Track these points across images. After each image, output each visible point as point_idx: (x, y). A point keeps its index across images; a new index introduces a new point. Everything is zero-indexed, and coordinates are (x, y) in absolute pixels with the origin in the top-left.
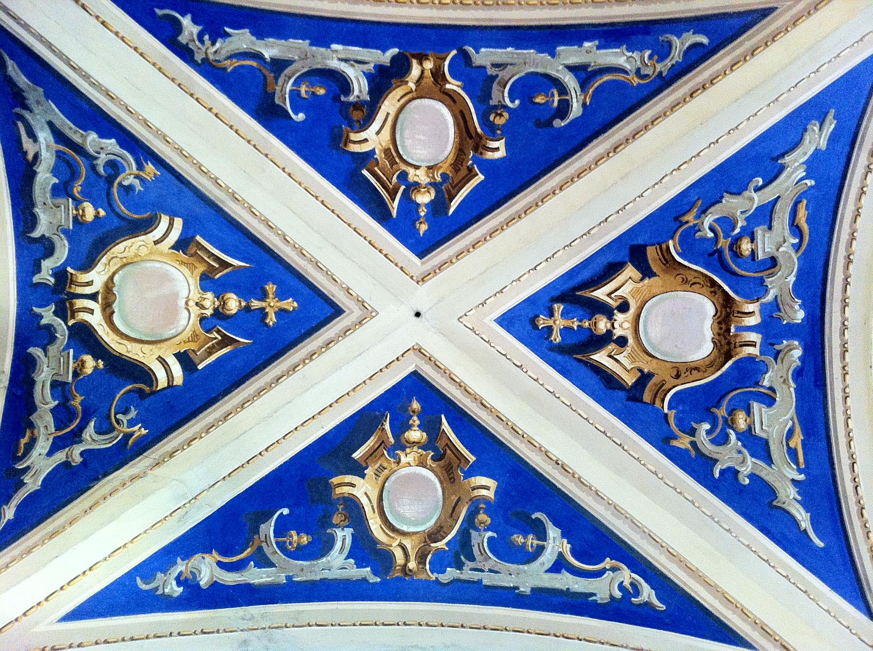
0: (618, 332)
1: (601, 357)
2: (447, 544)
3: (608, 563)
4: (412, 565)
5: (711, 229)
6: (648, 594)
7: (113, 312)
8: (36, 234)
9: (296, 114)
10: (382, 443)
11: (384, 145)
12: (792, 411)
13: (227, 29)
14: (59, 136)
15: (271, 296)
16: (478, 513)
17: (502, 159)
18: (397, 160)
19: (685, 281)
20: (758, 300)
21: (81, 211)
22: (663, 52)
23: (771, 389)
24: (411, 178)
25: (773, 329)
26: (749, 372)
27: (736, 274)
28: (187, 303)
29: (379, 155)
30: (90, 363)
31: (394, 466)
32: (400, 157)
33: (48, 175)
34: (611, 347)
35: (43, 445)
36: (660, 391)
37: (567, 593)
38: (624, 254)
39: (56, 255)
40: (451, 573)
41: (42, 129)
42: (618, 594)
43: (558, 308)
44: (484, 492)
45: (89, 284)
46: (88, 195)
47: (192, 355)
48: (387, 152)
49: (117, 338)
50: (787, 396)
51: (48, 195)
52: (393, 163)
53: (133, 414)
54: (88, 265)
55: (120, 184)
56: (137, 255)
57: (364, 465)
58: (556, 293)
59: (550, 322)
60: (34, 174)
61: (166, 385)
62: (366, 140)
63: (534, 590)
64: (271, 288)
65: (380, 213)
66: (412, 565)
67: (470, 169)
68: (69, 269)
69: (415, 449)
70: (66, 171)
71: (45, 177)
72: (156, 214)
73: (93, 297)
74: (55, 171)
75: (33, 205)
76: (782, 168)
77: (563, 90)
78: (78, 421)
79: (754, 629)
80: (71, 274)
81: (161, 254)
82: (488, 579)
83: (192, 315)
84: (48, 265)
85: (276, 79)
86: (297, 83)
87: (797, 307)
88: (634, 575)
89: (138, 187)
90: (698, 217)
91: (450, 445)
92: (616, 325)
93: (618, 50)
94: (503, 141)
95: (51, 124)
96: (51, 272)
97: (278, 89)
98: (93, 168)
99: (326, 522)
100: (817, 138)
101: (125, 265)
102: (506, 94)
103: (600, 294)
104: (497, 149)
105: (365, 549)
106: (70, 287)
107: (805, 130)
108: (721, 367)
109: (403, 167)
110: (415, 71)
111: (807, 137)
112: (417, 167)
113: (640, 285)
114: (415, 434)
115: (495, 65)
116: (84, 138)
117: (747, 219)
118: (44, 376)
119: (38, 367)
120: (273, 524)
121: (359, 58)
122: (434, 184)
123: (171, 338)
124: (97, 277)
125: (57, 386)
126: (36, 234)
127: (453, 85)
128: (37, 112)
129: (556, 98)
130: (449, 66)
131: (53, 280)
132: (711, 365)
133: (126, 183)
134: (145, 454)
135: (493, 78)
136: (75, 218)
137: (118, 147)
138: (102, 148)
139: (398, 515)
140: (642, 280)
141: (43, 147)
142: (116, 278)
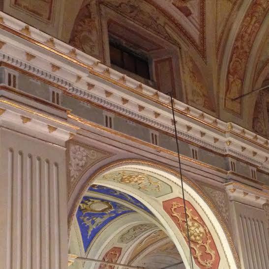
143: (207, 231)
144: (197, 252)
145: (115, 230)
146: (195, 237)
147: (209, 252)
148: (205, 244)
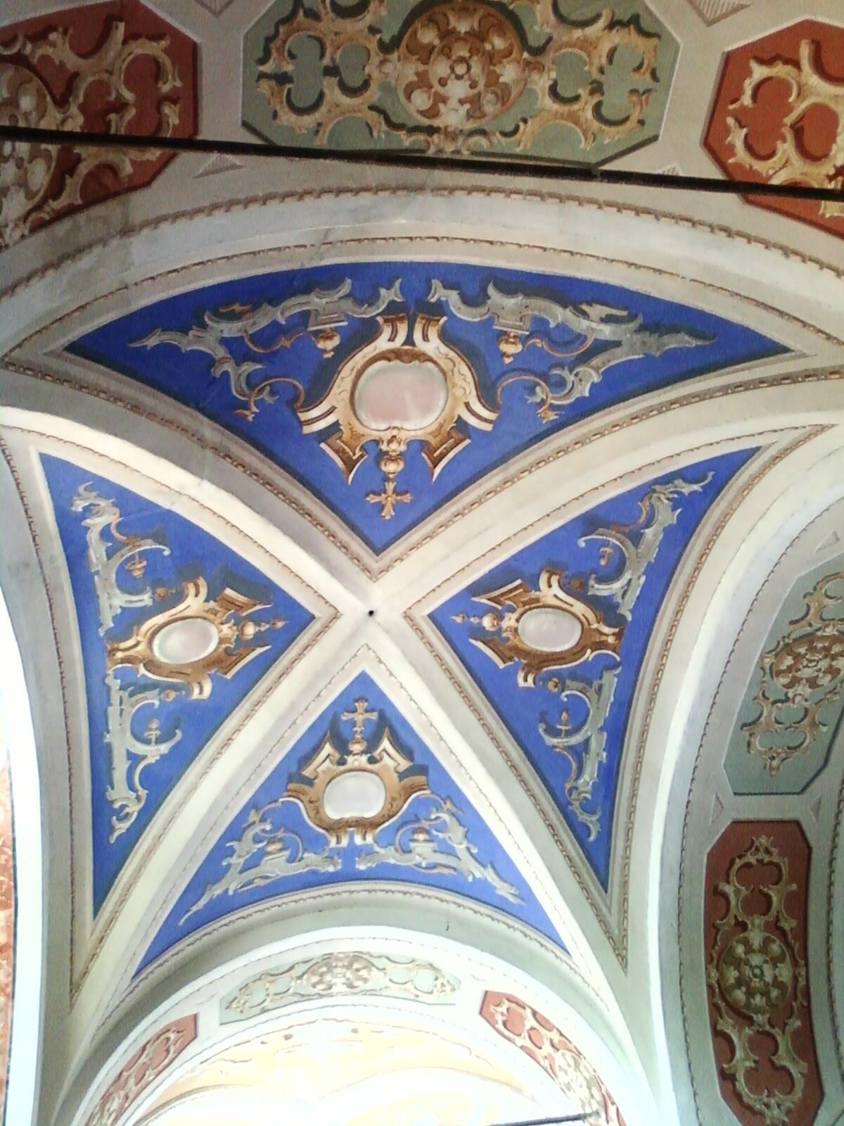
0: (350, 759)
1: (328, 749)
2: (143, 675)
3: (143, 793)
4: (120, 655)
5: (437, 818)
6: (122, 827)
7: (389, 360)
8: (491, 290)
9: (585, 541)
10: (241, 607)
11: (544, 599)
12: (282, 874)
13: (679, 511)
14: (602, 347)
15: (399, 498)
16: (176, 691)
17: (517, 685)
18: (527, 607)
19: (394, 799)
20: (376, 842)
21: (512, 340)
22: (587, 807)
23: (302, 859)
24: (508, 615)
25: (353, 852)
26: (314, 843)
27: (398, 830)
28: (394, 428)
29: (534, 594)
30: (330, 344)
31: (219, 621)
32: (530, 609)
33: (560, 319)
34: (337, 756)
35: (230, 329)
36: (297, 794)
37: (110, 769)
38: (419, 760)
39: (463, 307)
40: (115, 684)
41: (614, 333)
42: (117, 805)
43: (374, 716)
44: (196, 691)
45: (425, 338)
46: (529, 351)
47: (339, 435)
48: (537, 600)
49: (359, 366)
50: (298, 869)
51: (536, 313)
52: (524, 604)
53: (270, 400)
54: (445, 337)
55: (539, 384)
56: (454, 385)
57: (218, 598)
58: (388, 714)
59: (360, 711)
60: (565, 306)
61: (302, 419)
62: (550, 586)
63: (109, 745)
64: (407, 498)
65: (477, 588)
66: (120, 655)
67: (511, 659)
68: (445, 319)
69: (237, 633)
70: (565, 339)
71: (558, 315)
72: (499, 409)
73: (409, 340)
74: (562, 327)
75: (527, 295)
76: (484, 866)
77: (569, 734)
78: (261, 351)
79: (111, 913)
80: (438, 321)
81: (453, 408)
82: (113, 711)
83: (381, 433)
84: (453, 297)
85: (624, 534)
86: (615, 547)
87: (369, 865)
88: (135, 815)
89: (531, 400)
90: (448, 810)
91: (242, 657)
92: (356, 757)
93: (596, 775)
94: (532, 685)
95: (617, 344)
96: (443, 299)
97: (613, 533)
98: (561, 365)
99: (156, 584)
100: (504, 890)
101: (444, 373)
102: (574, 692)
103: (386, 744)
104: (526, 680)
105: (130, 620)
106: (423, 318)
107: (512, 885)
108: (320, 827)
109: (520, 610)
110: (606, 630)
111: (506, 885)
112: (518, 620)
113: (392, 770)
114: (250, 630)
115: (600, 687)
116: (597, 369)
117: (444, 839)
118: (316, 301)
119: (326, 292)
120: (153, 547)
121: (629, 593)
122: (500, 630)
123: (358, 419)
124: (433, 346)
125: (305, 317)
126: (491, 290)
127: (589, 655)
128: (635, 337)
129: (563, 728)
130: (607, 655)
131: (433, 300)
132: (321, 820)
133: (538, 389)
134: (226, 431)
135: (590, 684)
136: (506, 333)
137: (578, 395)
138: (581, 380)
139: (170, 633)
140: (397, 772)
141: (594, 325)
142: (430, 365)
143: (802, 983)
144: (739, 1054)
145: (405, 802)
146: (750, 993)
147: (786, 1063)
148: (776, 1031)
